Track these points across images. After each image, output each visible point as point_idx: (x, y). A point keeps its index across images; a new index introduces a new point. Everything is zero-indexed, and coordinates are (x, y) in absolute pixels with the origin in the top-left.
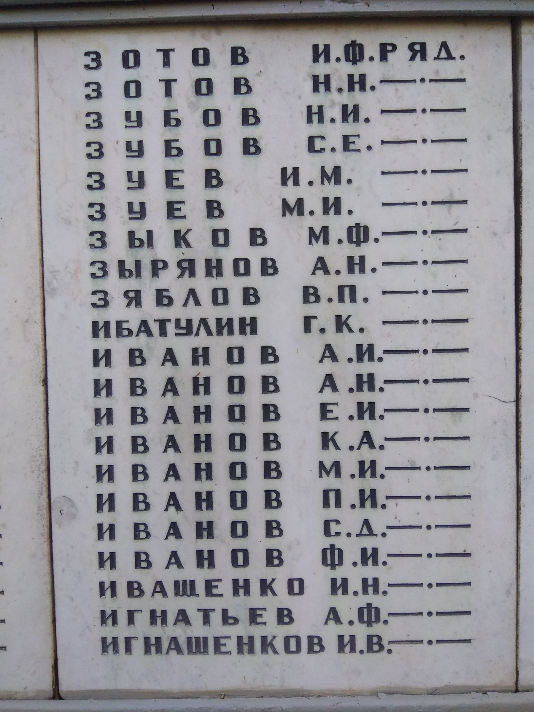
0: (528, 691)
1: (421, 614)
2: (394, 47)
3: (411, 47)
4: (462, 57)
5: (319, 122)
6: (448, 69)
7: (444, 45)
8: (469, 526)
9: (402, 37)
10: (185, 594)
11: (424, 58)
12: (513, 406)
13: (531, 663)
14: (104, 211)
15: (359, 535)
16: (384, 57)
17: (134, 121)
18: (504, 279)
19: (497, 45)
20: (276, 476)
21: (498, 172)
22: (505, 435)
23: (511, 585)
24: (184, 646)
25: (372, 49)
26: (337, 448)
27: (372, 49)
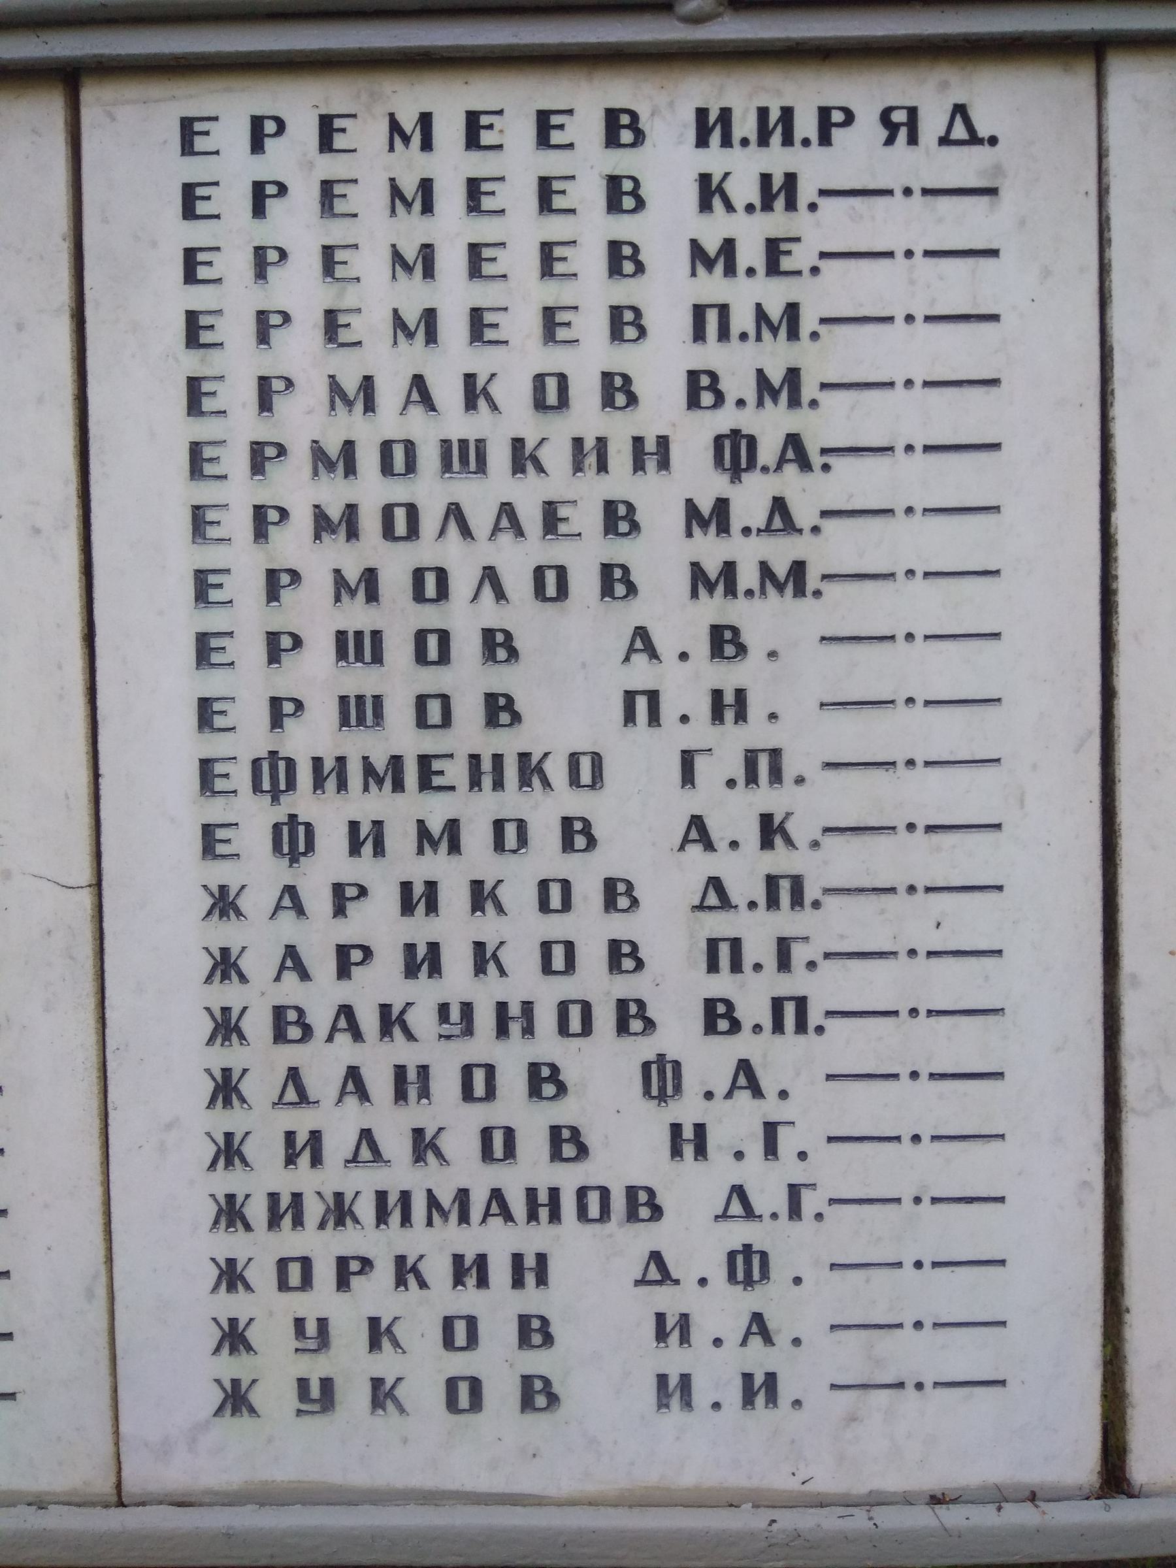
0: (143, 1504)
1: (891, 384)
2: (849, 118)
3: (885, 117)
4: (993, 141)
5: (720, 340)
6: (964, 166)
7: (960, 110)
8: (1003, 1324)
9: (866, 92)
10: (361, 721)
11: (913, 140)
12: (86, 899)
13: (146, 1445)
14: (560, 1078)
15: (768, 529)
16: (825, 139)
17: (314, 1401)
18: (58, 626)
19: (34, 131)
20: (276, 193)
21: (40, 400)
22: (72, 958)
23: (95, 1277)
24: (518, 1207)
25: (806, 125)
26: (729, 207)
27: (806, 125)
